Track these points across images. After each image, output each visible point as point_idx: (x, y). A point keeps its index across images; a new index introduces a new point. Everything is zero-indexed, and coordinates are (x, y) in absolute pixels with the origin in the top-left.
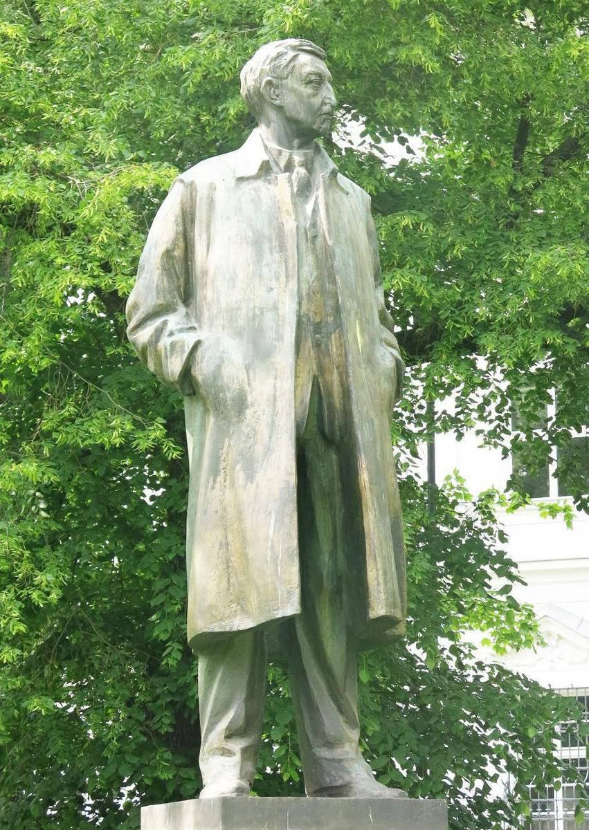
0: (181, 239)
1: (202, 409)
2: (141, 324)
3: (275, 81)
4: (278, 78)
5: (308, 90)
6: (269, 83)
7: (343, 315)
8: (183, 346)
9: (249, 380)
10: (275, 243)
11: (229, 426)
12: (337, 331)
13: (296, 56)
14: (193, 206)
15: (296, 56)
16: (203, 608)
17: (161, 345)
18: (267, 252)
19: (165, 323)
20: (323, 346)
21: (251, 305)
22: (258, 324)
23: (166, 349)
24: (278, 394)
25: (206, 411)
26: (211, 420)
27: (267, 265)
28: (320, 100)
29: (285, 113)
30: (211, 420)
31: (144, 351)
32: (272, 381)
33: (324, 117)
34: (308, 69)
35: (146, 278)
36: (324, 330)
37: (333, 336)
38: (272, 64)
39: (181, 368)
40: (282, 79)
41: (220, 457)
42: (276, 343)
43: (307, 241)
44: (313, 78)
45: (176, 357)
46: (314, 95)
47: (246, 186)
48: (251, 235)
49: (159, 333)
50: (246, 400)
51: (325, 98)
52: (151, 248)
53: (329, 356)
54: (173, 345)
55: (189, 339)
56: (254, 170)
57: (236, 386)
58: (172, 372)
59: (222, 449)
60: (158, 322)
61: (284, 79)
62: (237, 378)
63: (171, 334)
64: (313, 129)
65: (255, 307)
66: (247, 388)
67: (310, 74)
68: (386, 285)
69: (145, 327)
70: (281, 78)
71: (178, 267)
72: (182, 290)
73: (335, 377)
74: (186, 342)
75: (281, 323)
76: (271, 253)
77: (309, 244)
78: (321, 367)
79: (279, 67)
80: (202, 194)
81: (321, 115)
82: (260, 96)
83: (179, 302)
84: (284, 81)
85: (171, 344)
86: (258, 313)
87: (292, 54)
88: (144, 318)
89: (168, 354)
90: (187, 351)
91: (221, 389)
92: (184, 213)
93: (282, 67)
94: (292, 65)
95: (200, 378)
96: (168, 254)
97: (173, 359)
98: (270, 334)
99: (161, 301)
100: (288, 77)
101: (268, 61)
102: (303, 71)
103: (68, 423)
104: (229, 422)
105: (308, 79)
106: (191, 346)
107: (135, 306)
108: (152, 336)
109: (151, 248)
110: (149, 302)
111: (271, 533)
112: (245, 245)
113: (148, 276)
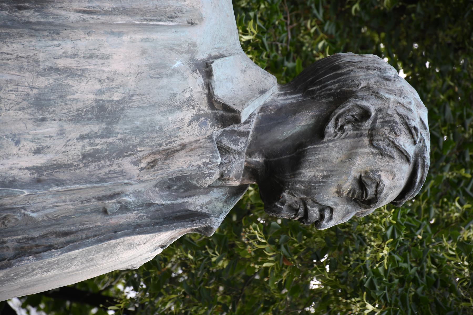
3: (367, 124)
4: (373, 129)
6: (365, 114)
7: (65, 58)
10: (100, 144)
13: (408, 160)
16: (9, 217)
18: (86, 129)
27: (62, 133)
28: (330, 204)
29: (312, 143)
33: (301, 210)
34: (386, 180)
38: (397, 118)
40: (371, 137)
43: (100, 199)
44: (371, 191)
48: (116, 97)
51: (332, 210)
61: (371, 142)
64: (282, 190)
67: (377, 186)
76: (82, 138)
77: (95, 203)
78: (401, 115)
79: (393, 130)
81: (305, 205)
84: (366, 140)
87: (411, 150)
93: (392, 137)
100: (375, 147)
101: (402, 110)
102: (383, 174)
105: (369, 182)
111: (408, 254)
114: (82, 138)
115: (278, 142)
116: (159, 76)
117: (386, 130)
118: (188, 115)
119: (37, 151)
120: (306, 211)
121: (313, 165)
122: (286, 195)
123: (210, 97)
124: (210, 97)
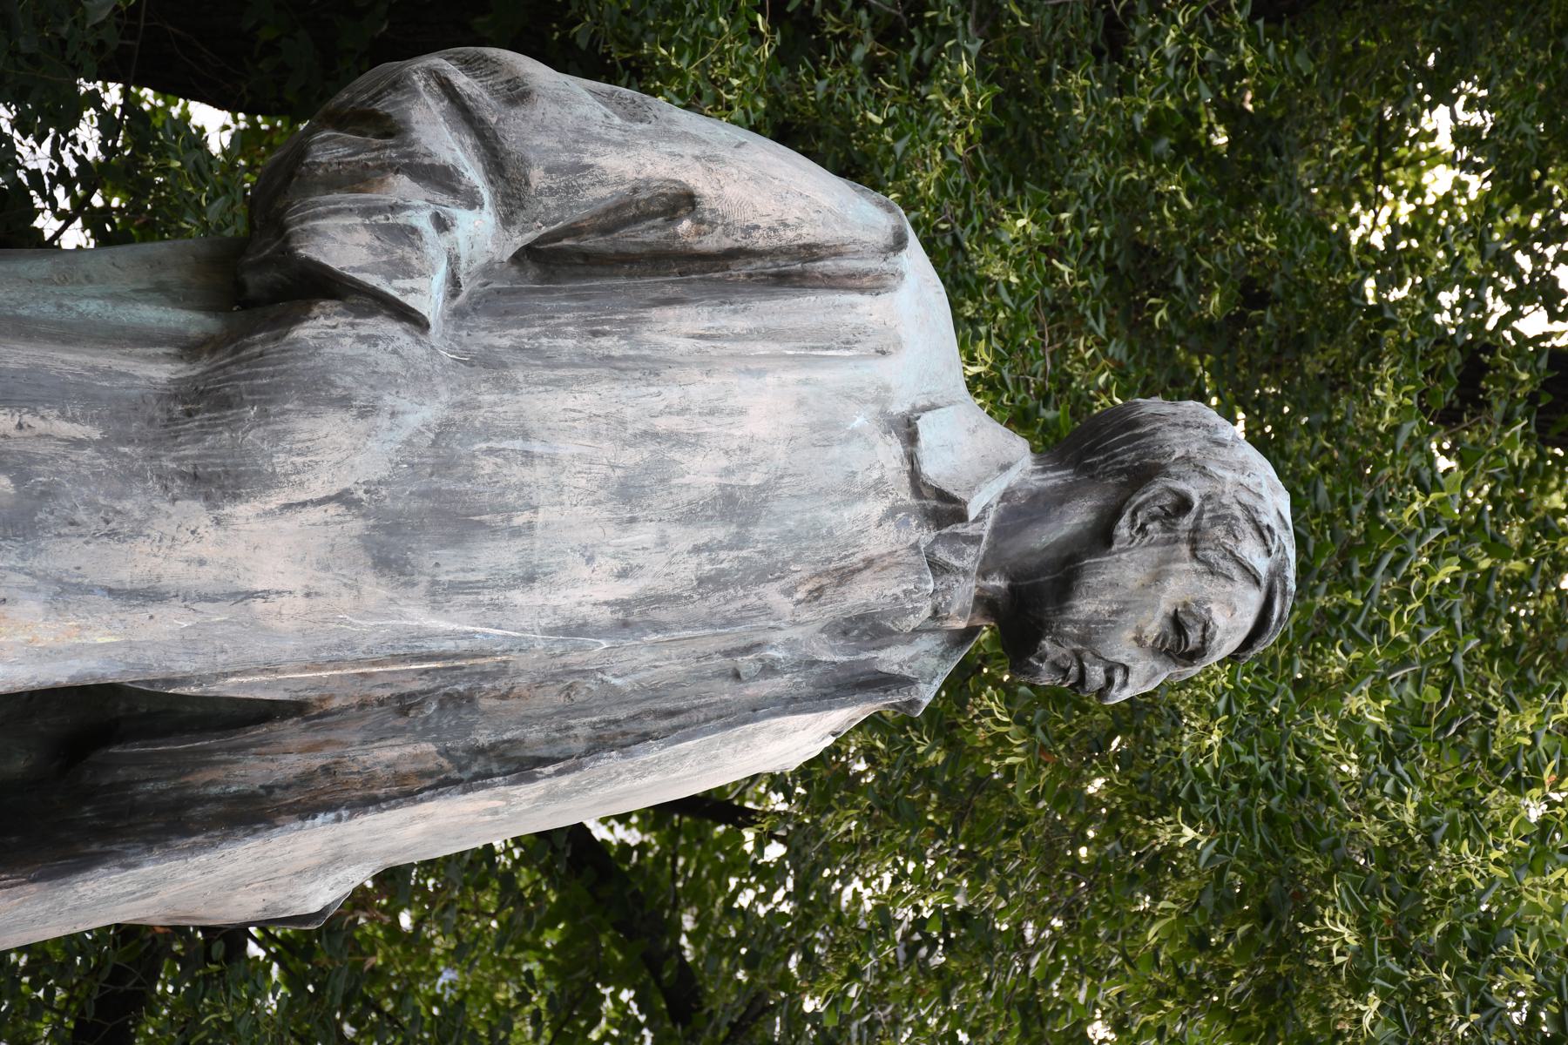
0: (728, 243)
1: (194, 331)
2: (464, 113)
3: (1187, 522)
5: (1154, 626)
8: (408, 273)
9: (304, 504)
10: (727, 560)
11: (143, 441)
12: (444, 762)
13: (1257, 583)
14: (833, 283)
15: (1257, 583)
17: (401, 186)
18: (703, 536)
19: (473, 202)
20: (401, 722)
21: (541, 497)
22: (481, 524)
23: (394, 208)
24: (258, 605)
25: (189, 349)
26: (161, 372)
27: (663, 542)
28: (1123, 659)
29: (1091, 554)
30: (161, 372)
31: (390, 129)
32: (295, 583)
33: (1074, 670)
34: (1220, 618)
35: (610, 126)
36: (448, 721)
37: (430, 747)
38: (1237, 511)
39: (334, 266)
40: (1194, 543)
41: (35, 412)
42: (424, 581)
43: (727, 654)
44: (1194, 637)
45: (370, 247)
46: (1139, 640)
47: (891, 452)
48: (754, 479)
49: (442, 178)
50: (236, 497)
51: (1126, 670)
52: (697, 140)
53: (364, 742)
54: (409, 234)
55: (429, 298)
56: (934, 469)
57: (281, 462)
58: (314, 231)
59: (62, 416)
60: (473, 174)
61: (1194, 551)
62: (311, 466)
63: (442, 224)
64: (1040, 637)
65: (535, 509)
66: (276, 500)
67: (1205, 628)
68: (327, 583)
69: (453, 128)
70: (1195, 540)
71: (648, 235)
72: (566, 242)
73: (291, 765)
74: (416, 283)
75: (485, 597)
76: (697, 550)
77: (719, 661)
79: (1231, 532)
80: (863, 309)
82: (1143, 474)
83: (530, 236)
84: (1185, 549)
85: (414, 230)
86: (519, 520)
88: (482, 121)
89: (381, 219)
90: (390, 289)
91: (268, 398)
92: (811, 252)
93: (1230, 543)
94: (1236, 573)
95: (305, 332)
96: (683, 202)
97: (365, 237)
98: (449, 564)
99: (537, 177)
100: (1200, 561)
101: (1246, 498)
102: (1214, 607)
103: (579, 261)
104: (157, 441)
105: (1190, 621)
106: (410, 301)
107: (517, 94)
108: (430, 155)
109: (697, 140)
110: (538, 140)
112: (724, 462)
113: (615, 135)
114: (697, 550)
115: (1032, 553)
116: (828, 443)
117: (1219, 531)
118: (877, 508)
119: (623, 574)
120: (1082, 671)
121: (1094, 593)
122: (1046, 644)
123: (915, 476)
124: (915, 476)
